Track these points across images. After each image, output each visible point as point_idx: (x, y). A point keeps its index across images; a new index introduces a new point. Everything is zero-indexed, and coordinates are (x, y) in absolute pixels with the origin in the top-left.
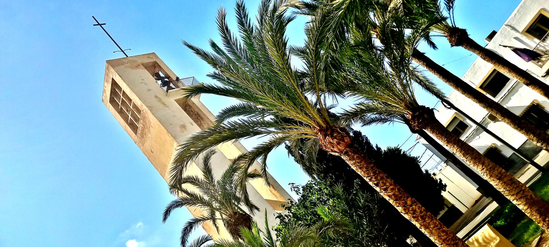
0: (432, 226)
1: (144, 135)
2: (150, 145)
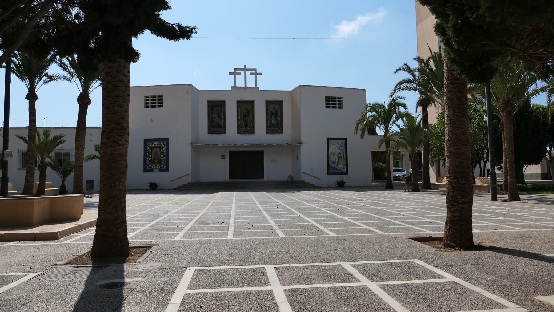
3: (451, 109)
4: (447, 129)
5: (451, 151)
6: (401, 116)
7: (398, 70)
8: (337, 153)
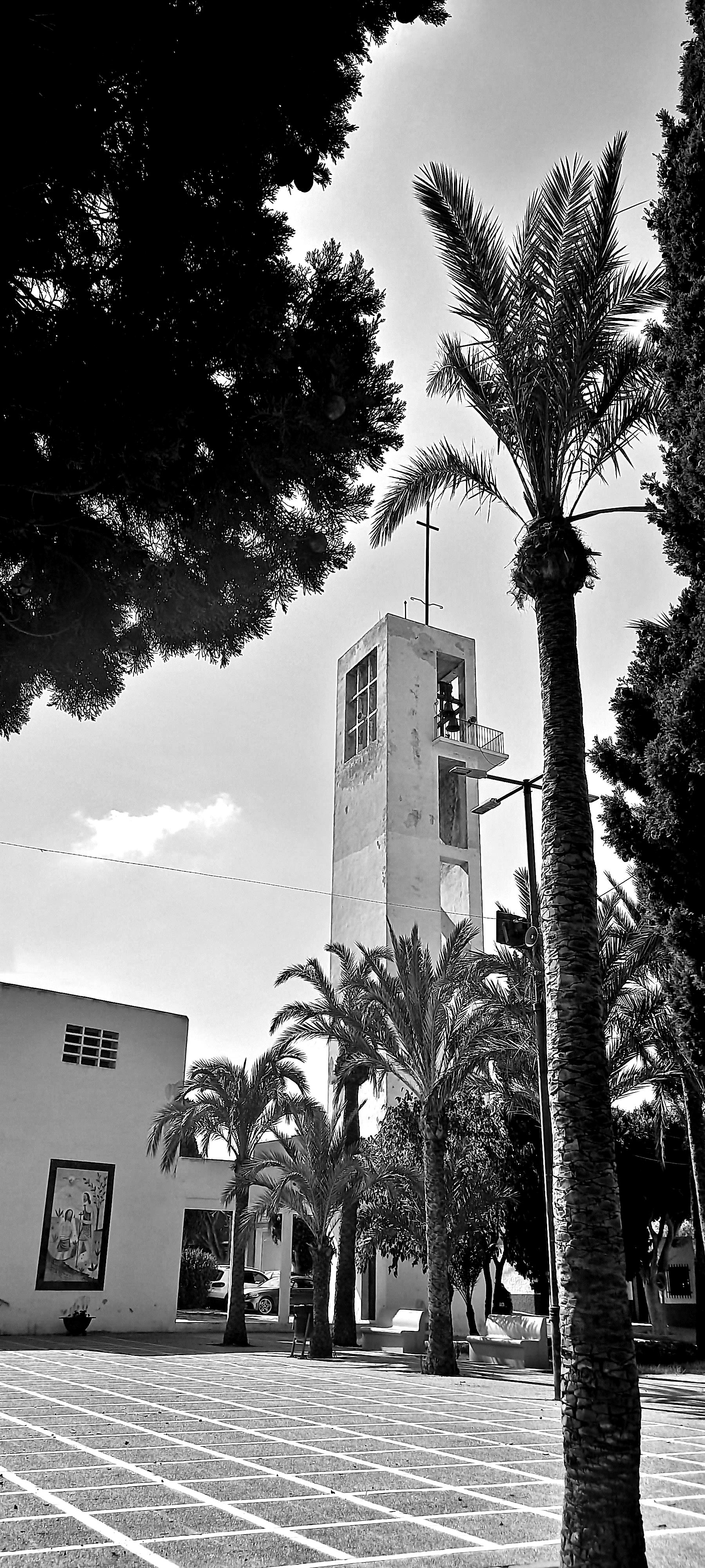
0: (435, 1261)
1: (355, 775)
2: (350, 798)
3: (575, 1135)
4: (563, 1194)
5: (576, 1268)
6: (287, 1108)
7: (286, 975)
8: (76, 1214)
